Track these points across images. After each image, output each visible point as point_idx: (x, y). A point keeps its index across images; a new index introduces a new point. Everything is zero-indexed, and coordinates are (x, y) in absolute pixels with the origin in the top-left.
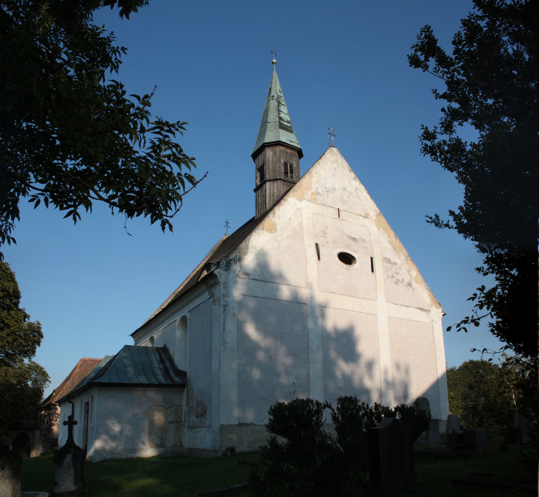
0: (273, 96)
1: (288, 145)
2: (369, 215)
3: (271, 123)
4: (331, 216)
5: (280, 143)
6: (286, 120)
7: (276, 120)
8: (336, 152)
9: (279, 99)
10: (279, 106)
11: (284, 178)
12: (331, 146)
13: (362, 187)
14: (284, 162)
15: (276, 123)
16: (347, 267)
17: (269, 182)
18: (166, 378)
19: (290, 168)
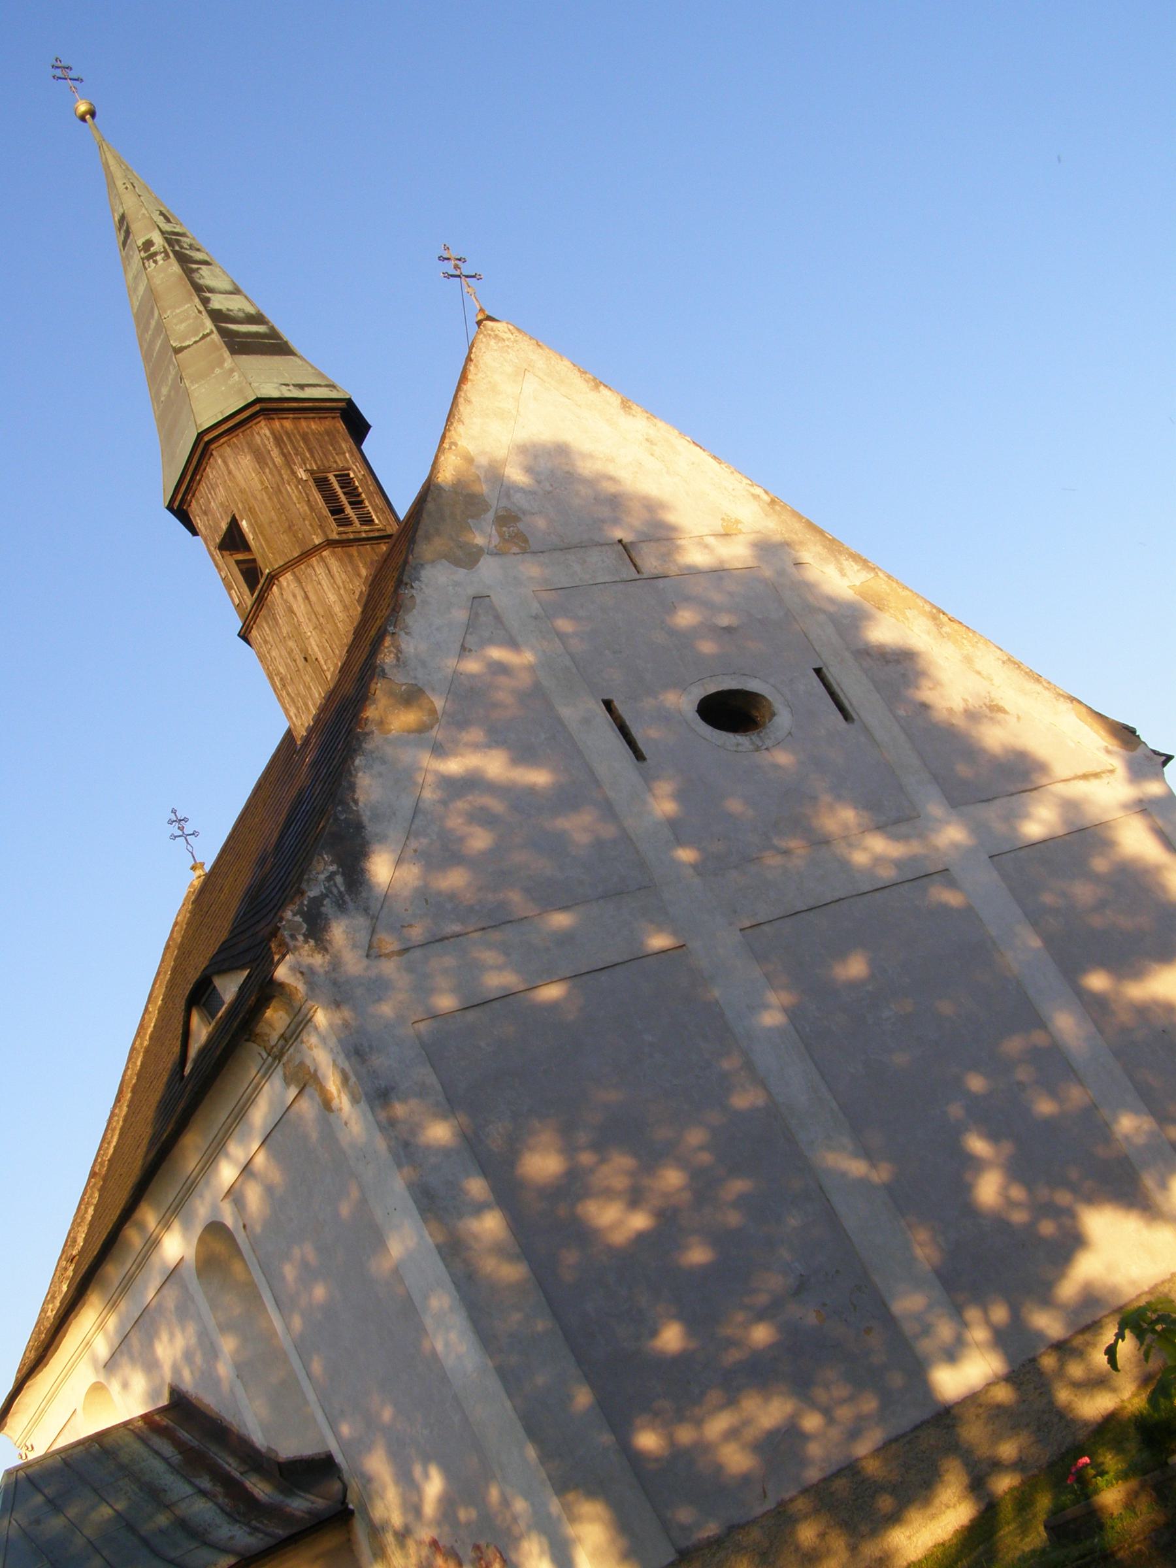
0: (149, 244)
1: (295, 405)
2: (737, 522)
3: (189, 346)
4: (607, 579)
5: (264, 405)
6: (241, 315)
7: (203, 325)
8: (510, 335)
9: (177, 248)
10: (189, 273)
11: (339, 533)
12: (479, 323)
13: (662, 431)
14: (311, 472)
15: (208, 339)
16: (753, 743)
17: (289, 576)
18: (254, 1523)
19: (342, 488)
